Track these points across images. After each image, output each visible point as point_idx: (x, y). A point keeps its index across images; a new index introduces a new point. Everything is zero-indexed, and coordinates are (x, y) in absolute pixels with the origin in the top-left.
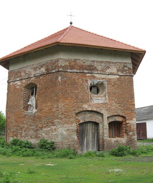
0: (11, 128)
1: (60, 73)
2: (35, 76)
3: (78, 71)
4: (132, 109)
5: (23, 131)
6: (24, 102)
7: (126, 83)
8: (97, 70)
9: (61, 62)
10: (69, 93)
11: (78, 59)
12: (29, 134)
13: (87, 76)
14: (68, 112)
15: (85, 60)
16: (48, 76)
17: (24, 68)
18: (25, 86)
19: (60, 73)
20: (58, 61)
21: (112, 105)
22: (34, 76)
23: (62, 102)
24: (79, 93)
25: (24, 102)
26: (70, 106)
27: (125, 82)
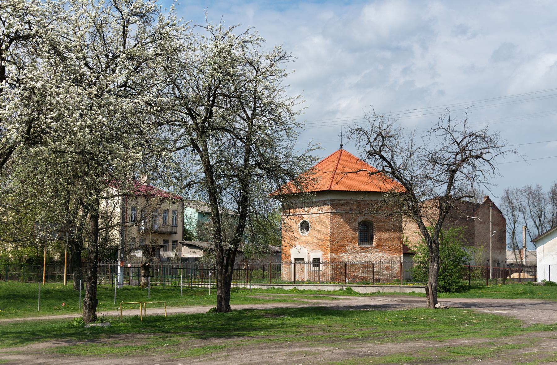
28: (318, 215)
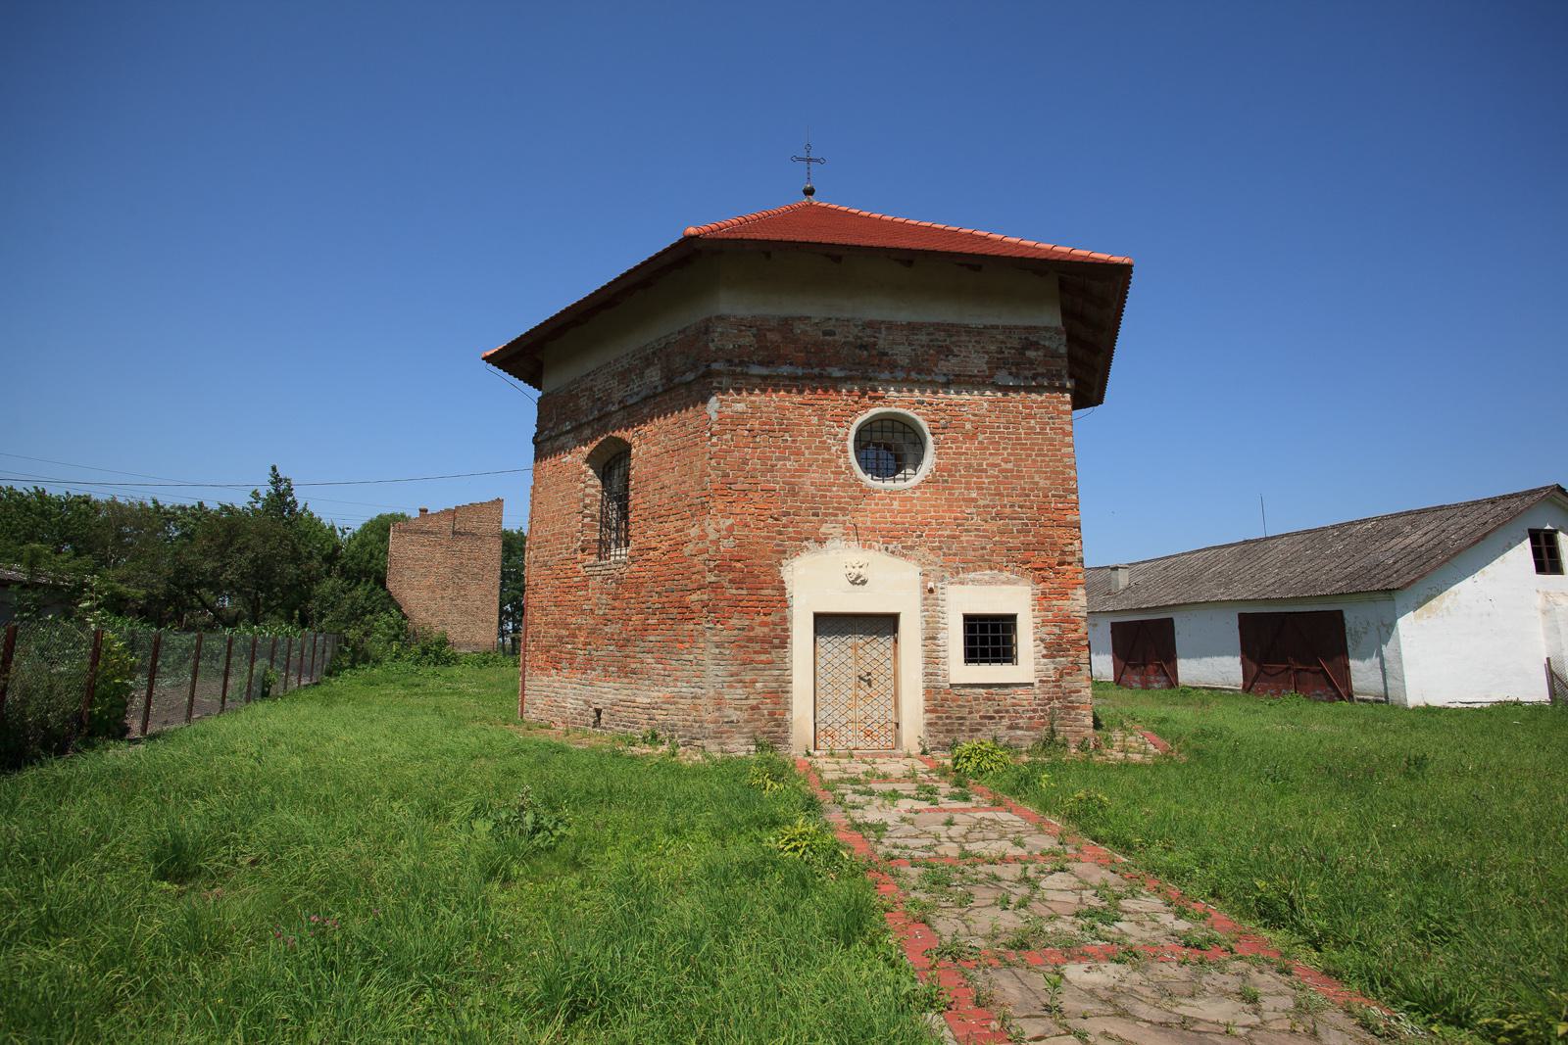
0: (539, 632)
2: (624, 408)
3: (800, 372)
5: (580, 646)
7: (1033, 421)
11: (799, 319)
15: (833, 322)
16: (670, 399)
17: (590, 378)
21: (962, 525)
22: (622, 405)
23: (721, 511)
27: (1029, 416)
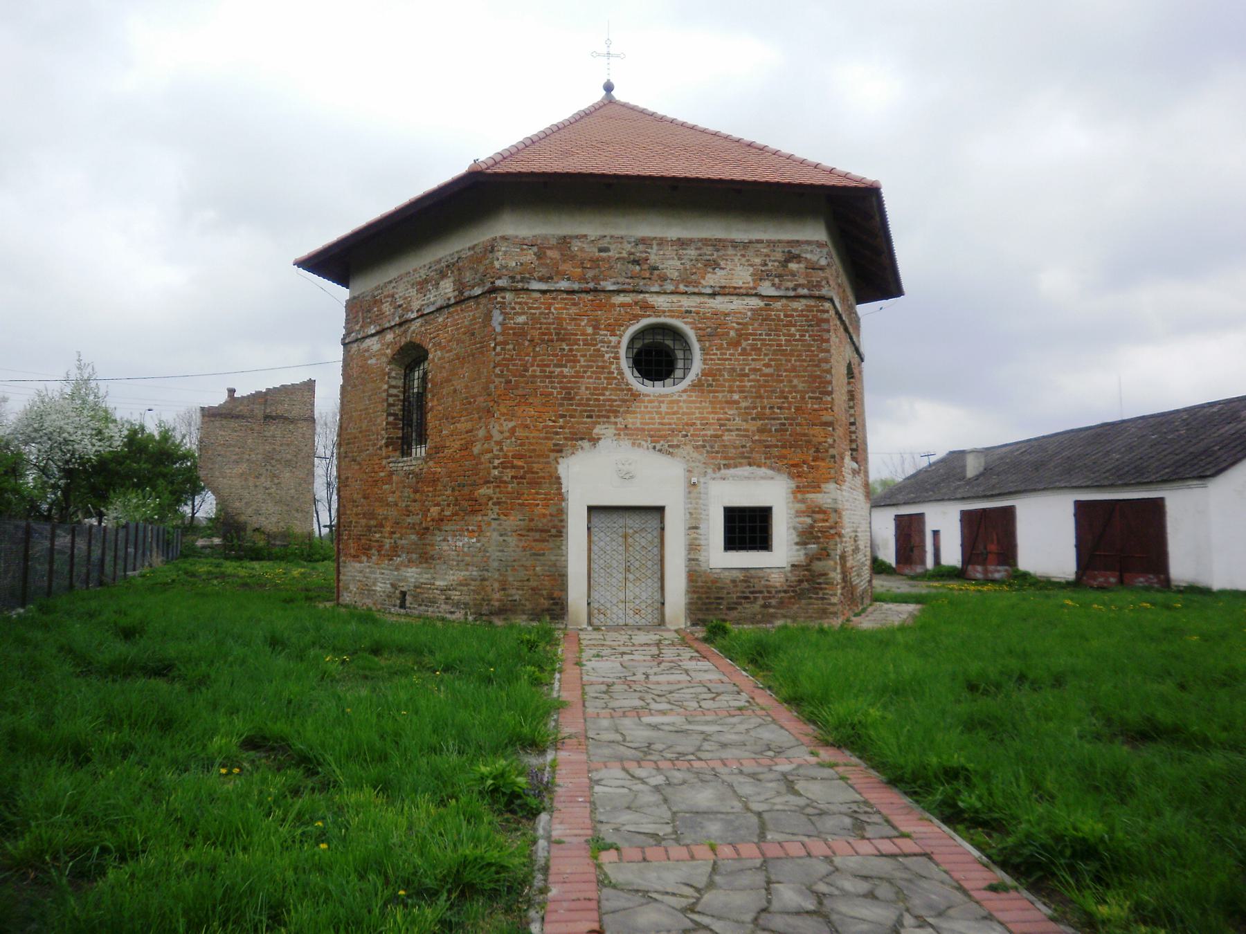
0: (351, 522)
1: (499, 299)
3: (576, 286)
4: (820, 443)
5: (387, 535)
6: (391, 419)
7: (793, 329)
8: (663, 279)
9: (505, 253)
10: (534, 376)
11: (577, 237)
12: (402, 548)
13: (614, 305)
14: (530, 457)
15: (608, 239)
18: (393, 358)
19: (499, 299)
20: (493, 248)
21: (724, 425)
23: (503, 414)
24: (578, 375)
25: (391, 419)
26: (536, 434)
27: (790, 324)
28: (755, 302)
